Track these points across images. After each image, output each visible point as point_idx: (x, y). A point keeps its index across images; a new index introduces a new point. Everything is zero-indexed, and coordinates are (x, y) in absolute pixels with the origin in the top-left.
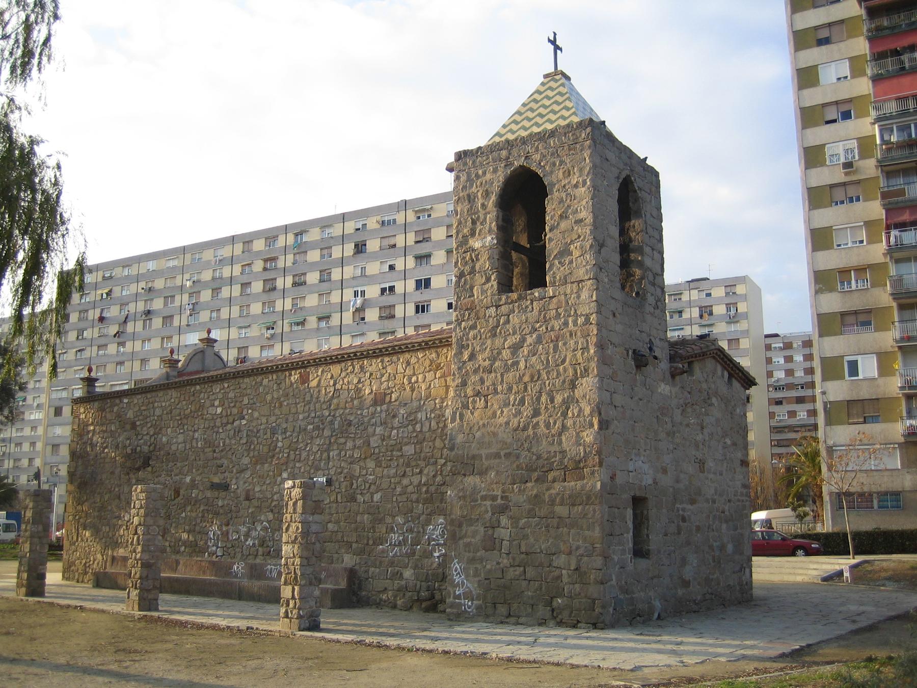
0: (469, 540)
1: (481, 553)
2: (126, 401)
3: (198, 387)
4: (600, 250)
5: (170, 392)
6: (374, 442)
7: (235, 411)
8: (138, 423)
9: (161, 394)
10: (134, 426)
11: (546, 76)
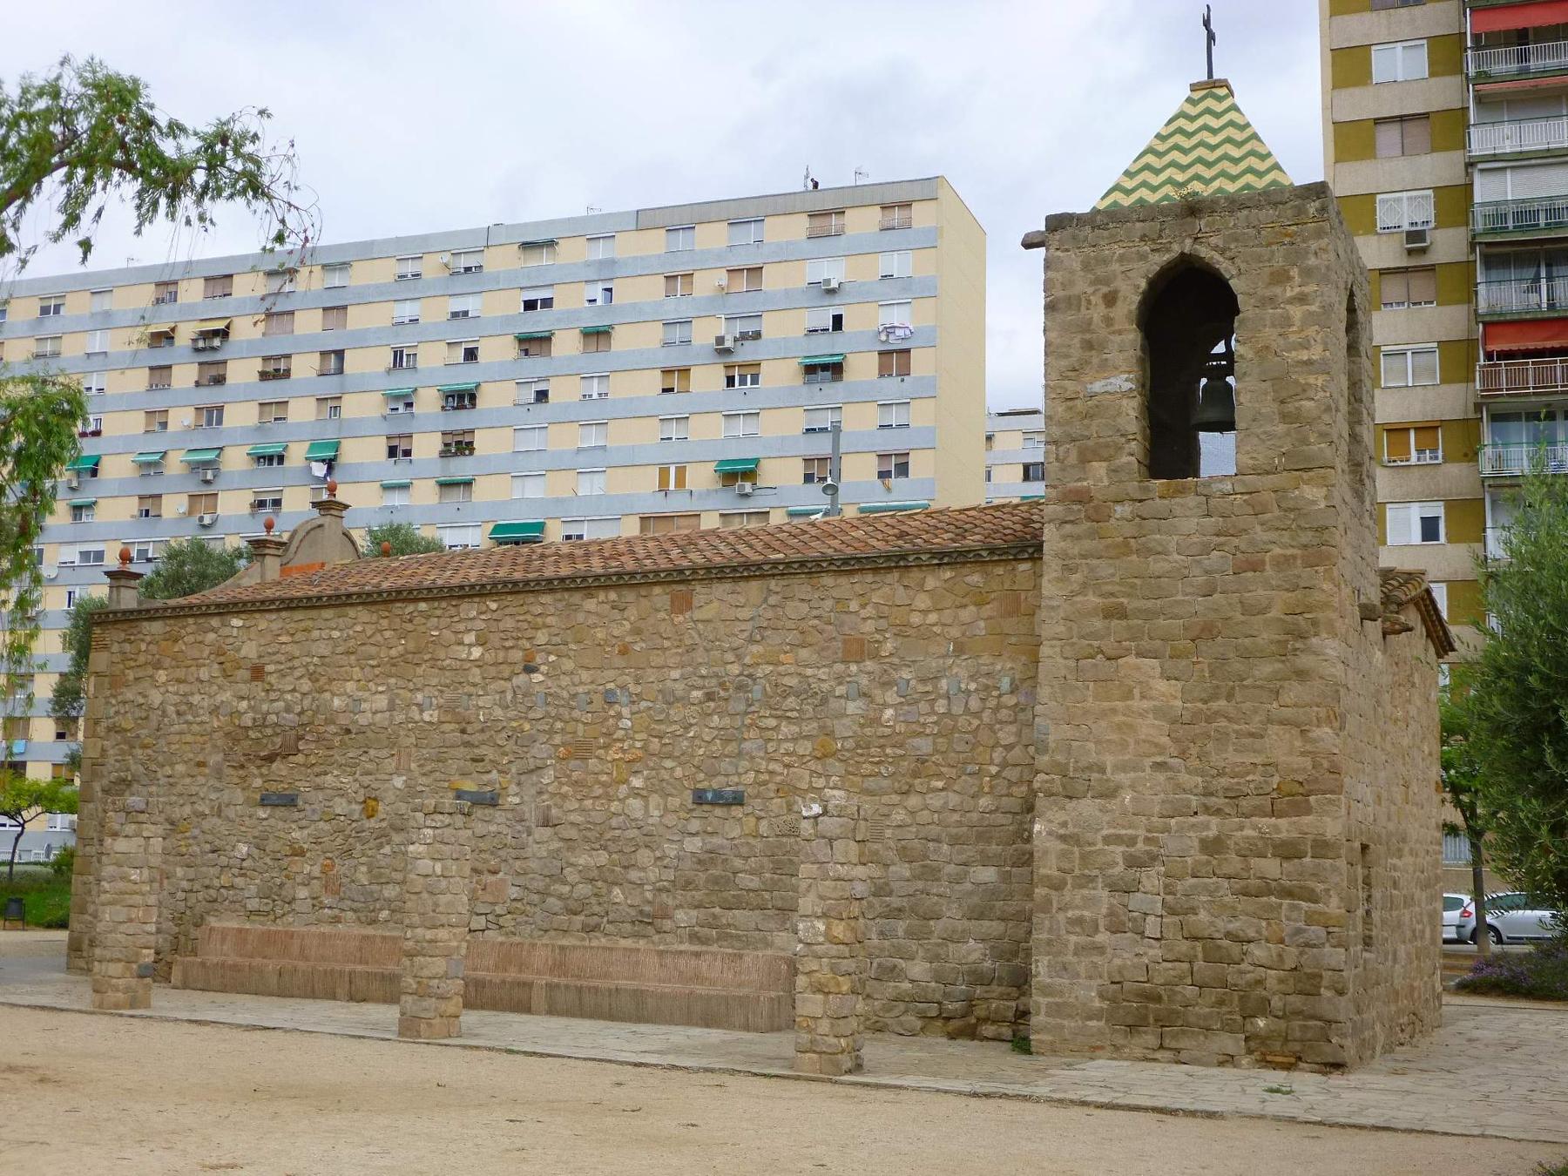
0: (1078, 913)
1: (1102, 937)
2: (236, 622)
3: (423, 606)
4: (140, 225)
5: (351, 612)
6: (843, 728)
7: (517, 655)
8: (269, 668)
9: (328, 613)
10: (258, 673)
11: (1194, 87)
